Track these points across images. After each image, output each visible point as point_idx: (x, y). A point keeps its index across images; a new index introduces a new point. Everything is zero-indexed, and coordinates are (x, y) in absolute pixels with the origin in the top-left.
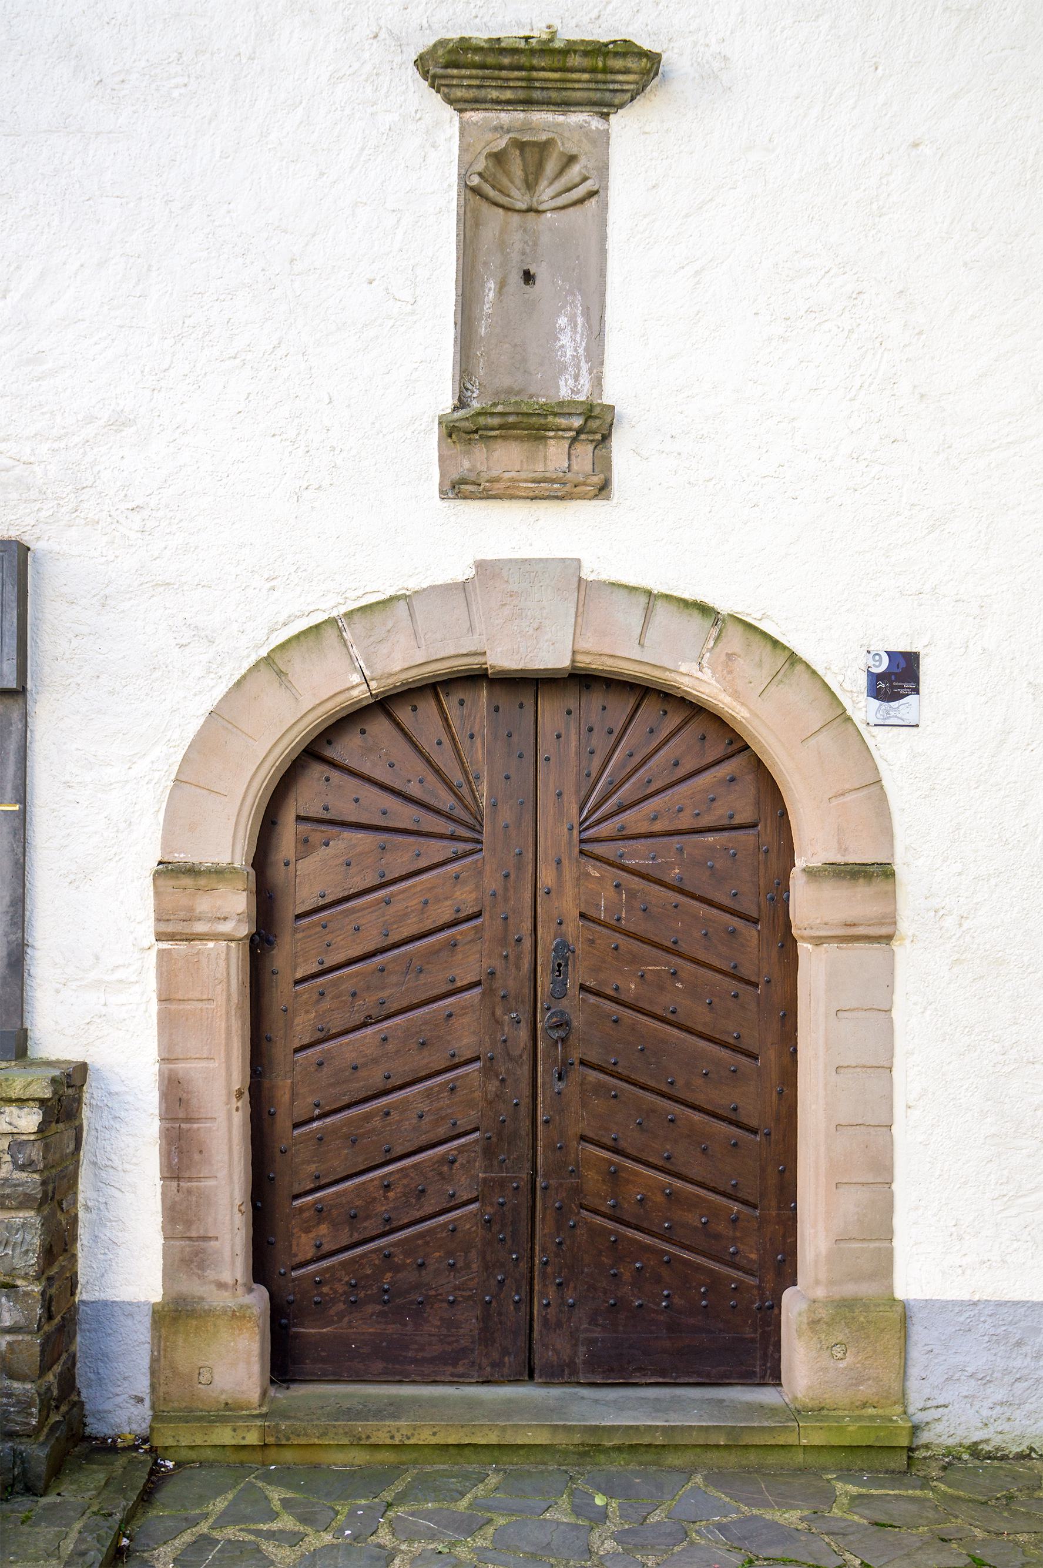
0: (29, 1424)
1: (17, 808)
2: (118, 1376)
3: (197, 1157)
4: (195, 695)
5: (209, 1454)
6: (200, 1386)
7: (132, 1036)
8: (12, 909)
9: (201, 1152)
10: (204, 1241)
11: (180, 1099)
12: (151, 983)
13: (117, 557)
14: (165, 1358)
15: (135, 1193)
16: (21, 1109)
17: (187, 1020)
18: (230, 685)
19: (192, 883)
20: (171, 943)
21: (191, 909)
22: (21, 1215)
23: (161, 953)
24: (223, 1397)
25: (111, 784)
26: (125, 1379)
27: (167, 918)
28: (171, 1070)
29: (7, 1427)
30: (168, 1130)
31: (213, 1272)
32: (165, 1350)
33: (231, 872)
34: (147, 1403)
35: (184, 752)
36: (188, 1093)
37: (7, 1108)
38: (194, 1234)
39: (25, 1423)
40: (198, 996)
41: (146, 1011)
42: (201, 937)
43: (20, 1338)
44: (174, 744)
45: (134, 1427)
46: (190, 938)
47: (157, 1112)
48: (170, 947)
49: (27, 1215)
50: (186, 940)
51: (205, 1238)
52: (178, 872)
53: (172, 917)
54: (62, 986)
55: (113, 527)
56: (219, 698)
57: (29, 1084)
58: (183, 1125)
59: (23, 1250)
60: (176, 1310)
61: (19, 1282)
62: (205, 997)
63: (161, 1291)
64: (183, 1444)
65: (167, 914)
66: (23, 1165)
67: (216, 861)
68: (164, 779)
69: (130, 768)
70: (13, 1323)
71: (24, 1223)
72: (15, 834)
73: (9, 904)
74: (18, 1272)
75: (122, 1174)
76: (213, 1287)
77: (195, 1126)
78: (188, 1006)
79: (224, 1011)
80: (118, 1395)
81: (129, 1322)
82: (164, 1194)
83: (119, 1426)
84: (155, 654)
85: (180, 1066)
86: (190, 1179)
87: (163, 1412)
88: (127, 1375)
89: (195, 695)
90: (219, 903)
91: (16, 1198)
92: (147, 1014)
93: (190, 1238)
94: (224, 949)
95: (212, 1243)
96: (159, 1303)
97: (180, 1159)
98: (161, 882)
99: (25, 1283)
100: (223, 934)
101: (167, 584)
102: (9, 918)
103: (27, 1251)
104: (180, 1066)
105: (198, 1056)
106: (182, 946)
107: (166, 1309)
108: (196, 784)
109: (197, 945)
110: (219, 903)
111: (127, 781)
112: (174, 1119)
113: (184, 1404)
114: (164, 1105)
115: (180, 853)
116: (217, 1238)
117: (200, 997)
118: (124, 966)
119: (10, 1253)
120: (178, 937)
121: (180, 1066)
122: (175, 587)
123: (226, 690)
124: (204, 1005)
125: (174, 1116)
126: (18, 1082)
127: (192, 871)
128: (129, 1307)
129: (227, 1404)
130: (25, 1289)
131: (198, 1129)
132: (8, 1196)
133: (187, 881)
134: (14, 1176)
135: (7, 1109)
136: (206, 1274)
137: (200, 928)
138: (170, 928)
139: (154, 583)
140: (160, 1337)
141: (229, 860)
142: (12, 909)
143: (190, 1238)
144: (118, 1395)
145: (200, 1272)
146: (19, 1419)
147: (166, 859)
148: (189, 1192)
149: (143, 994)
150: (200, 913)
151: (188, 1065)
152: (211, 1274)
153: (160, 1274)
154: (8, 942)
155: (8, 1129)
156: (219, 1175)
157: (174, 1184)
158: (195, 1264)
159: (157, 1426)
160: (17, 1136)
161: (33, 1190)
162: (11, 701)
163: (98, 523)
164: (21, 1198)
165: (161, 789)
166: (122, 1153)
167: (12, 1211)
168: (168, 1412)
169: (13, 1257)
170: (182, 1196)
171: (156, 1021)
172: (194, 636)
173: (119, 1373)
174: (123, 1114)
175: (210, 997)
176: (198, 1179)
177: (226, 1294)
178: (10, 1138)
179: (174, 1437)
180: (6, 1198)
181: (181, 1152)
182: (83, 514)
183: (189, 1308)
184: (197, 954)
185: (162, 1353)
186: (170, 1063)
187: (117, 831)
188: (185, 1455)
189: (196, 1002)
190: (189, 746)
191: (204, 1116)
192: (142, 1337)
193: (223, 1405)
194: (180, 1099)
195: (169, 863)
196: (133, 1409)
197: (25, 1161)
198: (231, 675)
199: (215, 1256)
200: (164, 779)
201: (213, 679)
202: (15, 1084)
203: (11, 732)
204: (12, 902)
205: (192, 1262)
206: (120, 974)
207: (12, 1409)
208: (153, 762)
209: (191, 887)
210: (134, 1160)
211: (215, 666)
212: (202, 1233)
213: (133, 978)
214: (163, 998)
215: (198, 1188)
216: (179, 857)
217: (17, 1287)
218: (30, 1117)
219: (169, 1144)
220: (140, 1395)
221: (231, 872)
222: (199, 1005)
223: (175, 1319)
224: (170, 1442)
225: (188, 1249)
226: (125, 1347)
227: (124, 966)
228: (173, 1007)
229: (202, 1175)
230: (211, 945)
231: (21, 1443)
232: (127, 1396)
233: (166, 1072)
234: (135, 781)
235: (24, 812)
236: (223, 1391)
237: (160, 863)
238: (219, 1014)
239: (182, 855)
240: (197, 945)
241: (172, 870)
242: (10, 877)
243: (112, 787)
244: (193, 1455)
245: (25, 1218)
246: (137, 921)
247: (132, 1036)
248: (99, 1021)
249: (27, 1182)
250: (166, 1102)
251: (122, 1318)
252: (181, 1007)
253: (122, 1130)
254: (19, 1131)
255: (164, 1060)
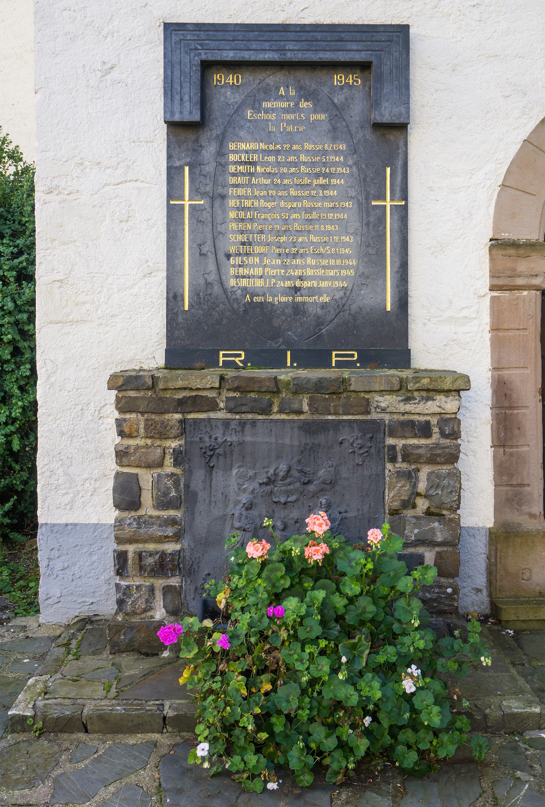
0: (453, 605)
1: (403, 203)
2: (465, 575)
3: (516, 432)
4: (514, 129)
5: (535, 625)
6: (523, 581)
7: (474, 353)
8: (401, 270)
9: (519, 428)
10: (520, 487)
11: (505, 394)
12: (486, 319)
13: (463, 38)
14: (500, 563)
15: (475, 456)
16: (448, 397)
17: (510, 342)
18: (538, 122)
19: (515, 252)
20: (499, 292)
21: (514, 270)
22: (445, 468)
23: (493, 299)
24: (538, 588)
25: (459, 188)
26: (469, 577)
27: (499, 275)
28: (499, 375)
29: (439, 608)
30: (497, 414)
31: (527, 507)
32: (500, 558)
33: (540, 245)
34: (485, 592)
35: (507, 167)
36: (511, 390)
37: (438, 397)
38: (514, 483)
39: (451, 605)
40: (517, 326)
41: (481, 337)
42: (520, 288)
43: (445, 549)
44: (499, 162)
45: (476, 608)
46: (512, 288)
47: (490, 403)
48: (498, 294)
49: (449, 468)
50: (509, 290)
51: (521, 485)
52: (505, 246)
53: (501, 275)
54: (427, 321)
55: (461, 18)
56: (530, 131)
57: (456, 380)
58: (507, 411)
59: (449, 491)
60: (507, 532)
61: (445, 512)
62: (521, 327)
63: (493, 520)
64: (521, 619)
65: (498, 273)
66: (449, 434)
67: (529, 238)
68: (493, 185)
69: (471, 178)
70: (443, 539)
71: (449, 473)
72: (403, 220)
73: (399, 266)
74: (445, 506)
75: (467, 443)
76: (527, 517)
77: (515, 412)
78: (511, 333)
79: (534, 337)
80: (464, 588)
81: (472, 540)
82: (495, 457)
83: (466, 608)
84: (488, 102)
85: (505, 372)
86: (512, 447)
87: (499, 598)
88: (470, 574)
89: (514, 129)
90: (532, 265)
91: (444, 457)
92: (482, 339)
93: (511, 485)
94: (534, 296)
95: (526, 488)
96: (492, 528)
97: (506, 434)
98: (494, 252)
99: (448, 513)
100: (534, 286)
101: (496, 56)
102: (399, 276)
103: (451, 492)
104: (505, 372)
105: (517, 366)
106: (507, 294)
107: (500, 531)
108: (516, 187)
109: (516, 293)
110: (532, 265)
111: (469, 187)
112: (501, 408)
113: (513, 593)
114: (495, 398)
115: (505, 233)
116: (529, 485)
117: (518, 327)
118: (468, 307)
119: (440, 493)
120: (505, 288)
121: (505, 372)
122: (501, 57)
123: (535, 126)
124: (521, 333)
125: (501, 406)
126: (448, 379)
127: (514, 245)
128: (472, 530)
129: (540, 593)
130: (449, 517)
131: (517, 414)
132: (439, 455)
133: (512, 251)
134: (441, 442)
135: (438, 397)
136: (522, 508)
137: (520, 281)
138: (500, 282)
139: (487, 55)
140: (496, 549)
141: (537, 238)
142: (401, 270)
143: (511, 485)
144: (464, 588)
145: (518, 507)
146: (447, 602)
147: (496, 237)
148: (511, 455)
149: (479, 326)
150: (520, 272)
151: (511, 372)
152: (525, 509)
153: (492, 509)
154: (399, 291)
155: (438, 410)
156: (530, 444)
157: (501, 450)
158: (515, 502)
159: (504, 607)
160: (443, 415)
161: (455, 451)
162: (399, 133)
163: (450, 15)
164: (447, 456)
165: (491, 191)
166: (467, 430)
167: (439, 465)
168: (503, 598)
169: (442, 496)
170: (507, 458)
171: (489, 344)
172: (514, 90)
173: (465, 573)
174: (467, 405)
175: (525, 327)
176: (517, 446)
177: (535, 521)
178: (438, 417)
179: (515, 614)
180: (438, 456)
181: (506, 428)
182: (440, 9)
183: (515, 530)
184: (516, 299)
185: (498, 560)
186: (498, 371)
187: (464, 219)
188: (519, 626)
189: (515, 331)
190: (511, 163)
191: (521, 405)
192: (480, 550)
193: (538, 594)
194: (505, 394)
195: (498, 240)
196: (474, 597)
197: (450, 431)
198: (538, 116)
199: (528, 496)
200: (493, 185)
201: (526, 118)
202: (446, 380)
203: (398, 154)
204: (401, 265)
205: (513, 500)
206: (464, 313)
207: (443, 596)
208: (486, 174)
209: (514, 255)
210: (475, 435)
211: (527, 110)
212: (519, 481)
213: (474, 316)
214: (494, 328)
215: (517, 452)
216: (505, 235)
217: (443, 515)
218: (453, 403)
219: (498, 423)
220: (479, 587)
221: (540, 245)
222: (518, 332)
223: (507, 538)
224: (513, 617)
225: (511, 492)
226: (469, 556)
227: (468, 307)
228: (501, 334)
229: (519, 444)
230: (525, 293)
231: (447, 618)
232: (470, 588)
233: (497, 376)
234: (474, 186)
235: (406, 206)
236: (538, 584)
237: (491, 240)
238: (531, 338)
239: (507, 235)
240: (516, 293)
241: (502, 244)
242: (399, 249)
243: (460, 190)
244: (524, 626)
245: (449, 470)
246: (476, 278)
247: (474, 353)
248: (452, 343)
249: (451, 446)
250: (496, 396)
251: (467, 538)
252: (506, 334)
253: (467, 415)
254: (445, 412)
255: (495, 369)
